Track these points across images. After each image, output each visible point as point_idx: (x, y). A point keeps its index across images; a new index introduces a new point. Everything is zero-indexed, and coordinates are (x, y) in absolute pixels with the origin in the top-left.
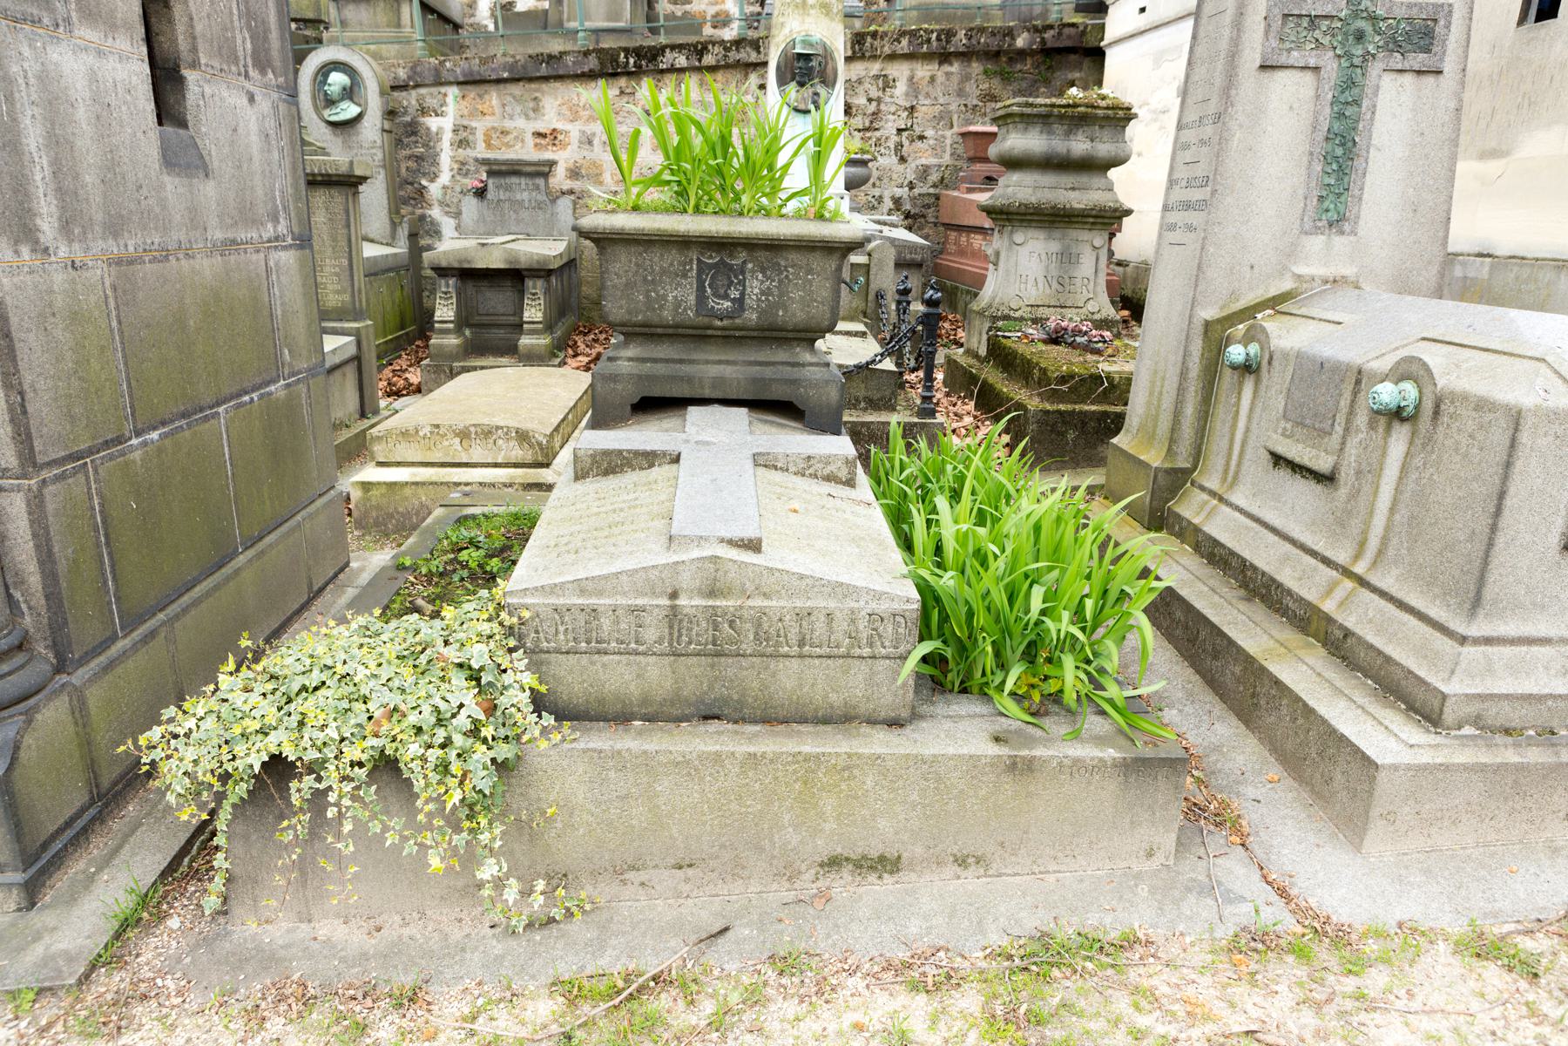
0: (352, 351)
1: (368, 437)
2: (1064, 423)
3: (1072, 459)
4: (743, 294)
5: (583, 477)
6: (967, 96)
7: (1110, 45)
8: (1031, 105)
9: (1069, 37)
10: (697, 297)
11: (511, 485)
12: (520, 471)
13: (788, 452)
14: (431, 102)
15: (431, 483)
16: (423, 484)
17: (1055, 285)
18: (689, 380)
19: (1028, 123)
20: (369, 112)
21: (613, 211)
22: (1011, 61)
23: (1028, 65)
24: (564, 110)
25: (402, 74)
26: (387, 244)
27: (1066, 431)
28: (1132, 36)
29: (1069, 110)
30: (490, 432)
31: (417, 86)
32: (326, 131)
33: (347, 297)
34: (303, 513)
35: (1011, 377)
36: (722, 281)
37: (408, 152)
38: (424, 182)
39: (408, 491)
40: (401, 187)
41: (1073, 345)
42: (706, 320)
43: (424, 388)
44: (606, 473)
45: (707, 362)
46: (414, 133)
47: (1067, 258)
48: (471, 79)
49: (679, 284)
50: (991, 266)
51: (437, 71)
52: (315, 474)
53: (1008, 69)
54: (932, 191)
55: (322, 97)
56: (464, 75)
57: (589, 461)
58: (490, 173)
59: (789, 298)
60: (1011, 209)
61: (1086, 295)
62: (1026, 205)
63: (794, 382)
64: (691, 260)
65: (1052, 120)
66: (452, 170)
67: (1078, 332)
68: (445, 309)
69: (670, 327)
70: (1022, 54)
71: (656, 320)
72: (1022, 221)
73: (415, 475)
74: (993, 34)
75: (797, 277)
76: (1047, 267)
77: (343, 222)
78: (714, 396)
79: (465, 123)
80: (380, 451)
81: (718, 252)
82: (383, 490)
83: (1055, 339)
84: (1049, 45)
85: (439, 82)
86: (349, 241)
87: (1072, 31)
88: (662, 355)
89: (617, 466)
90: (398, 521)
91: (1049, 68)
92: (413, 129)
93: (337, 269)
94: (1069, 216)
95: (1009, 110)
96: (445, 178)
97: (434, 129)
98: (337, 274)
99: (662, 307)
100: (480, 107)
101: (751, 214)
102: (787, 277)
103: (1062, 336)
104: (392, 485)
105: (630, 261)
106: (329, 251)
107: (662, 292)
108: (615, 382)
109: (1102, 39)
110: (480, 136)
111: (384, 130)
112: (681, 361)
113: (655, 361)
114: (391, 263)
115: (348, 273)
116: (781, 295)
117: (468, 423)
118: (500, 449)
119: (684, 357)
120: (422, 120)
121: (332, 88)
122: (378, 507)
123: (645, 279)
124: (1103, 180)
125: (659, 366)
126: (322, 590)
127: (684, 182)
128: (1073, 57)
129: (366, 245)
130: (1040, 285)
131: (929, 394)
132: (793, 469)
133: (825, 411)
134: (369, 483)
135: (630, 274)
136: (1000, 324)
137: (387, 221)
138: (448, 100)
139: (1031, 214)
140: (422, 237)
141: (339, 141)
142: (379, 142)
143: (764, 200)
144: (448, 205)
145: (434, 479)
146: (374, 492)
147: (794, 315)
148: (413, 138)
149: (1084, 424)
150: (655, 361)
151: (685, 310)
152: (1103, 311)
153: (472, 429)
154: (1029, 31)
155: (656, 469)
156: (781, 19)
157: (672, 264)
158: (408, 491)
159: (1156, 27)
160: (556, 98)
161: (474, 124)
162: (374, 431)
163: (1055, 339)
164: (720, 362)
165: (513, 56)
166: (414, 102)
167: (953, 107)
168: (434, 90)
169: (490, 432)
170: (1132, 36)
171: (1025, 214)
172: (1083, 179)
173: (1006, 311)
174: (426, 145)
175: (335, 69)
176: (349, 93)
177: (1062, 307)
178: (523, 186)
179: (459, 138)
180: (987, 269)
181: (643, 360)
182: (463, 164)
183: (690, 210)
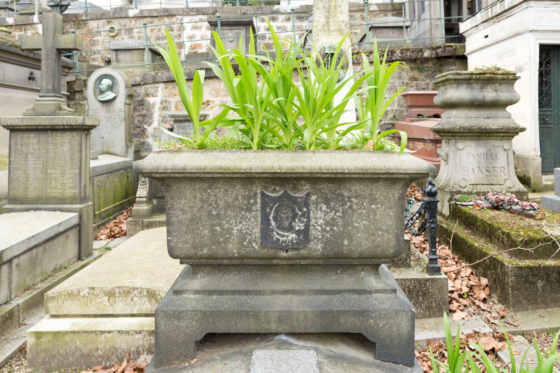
0: (76, 221)
1: (45, 297)
2: (534, 275)
3: (543, 301)
4: (307, 226)
6: (403, 79)
7: (470, 53)
8: (459, 74)
9: (449, 51)
10: (262, 230)
11: (140, 332)
14: (151, 91)
15: (84, 332)
16: (79, 332)
17: (485, 172)
18: (255, 315)
19: (458, 84)
20: (119, 96)
21: (179, 151)
22: (422, 63)
23: (430, 64)
24: (213, 92)
25: (138, 79)
26: (123, 156)
27: (536, 281)
28: (482, 48)
29: (481, 76)
30: (129, 292)
31: (145, 84)
32: (99, 105)
33: (76, 191)
35: (474, 233)
36: (286, 214)
37: (139, 113)
38: (145, 127)
40: (134, 129)
41: (510, 211)
42: (271, 252)
43: (128, 233)
45: (273, 292)
46: (142, 105)
47: (490, 156)
48: (170, 80)
49: (244, 218)
50: (442, 162)
51: (154, 78)
53: (421, 66)
54: (390, 122)
55: (98, 90)
56: (167, 79)
58: (175, 121)
59: (354, 227)
60: (455, 130)
61: (504, 177)
62: (463, 128)
63: (363, 313)
64: (256, 194)
65: (472, 81)
66: (159, 120)
67: (511, 203)
68: (142, 190)
69: (236, 258)
70: (427, 60)
71: (221, 253)
72: (461, 136)
73: (74, 325)
74: (413, 51)
75: (361, 206)
76: (479, 162)
77: (78, 150)
79: (166, 99)
80: (51, 305)
81: (282, 185)
82: (50, 337)
83: (497, 206)
84: (440, 55)
85: (155, 82)
86: (81, 160)
87: (450, 48)
88: (228, 286)
91: (440, 65)
92: (142, 103)
93: (72, 175)
94: (488, 133)
95: (448, 77)
96: (155, 124)
97: (151, 102)
98: (72, 178)
99: (226, 241)
100: (173, 92)
101: (312, 148)
102: (351, 207)
103: (502, 205)
104: (57, 334)
105: (195, 197)
106: (69, 165)
107: (226, 226)
108: (179, 319)
109: (465, 51)
110: (173, 105)
111: (126, 104)
112: (247, 293)
113: (221, 293)
114: (122, 166)
115: (78, 177)
116: (345, 225)
117: (114, 286)
118: (136, 304)
119: (251, 288)
120: (146, 99)
121: (103, 86)
122: (46, 351)
123: (210, 214)
124: (505, 113)
125: (226, 297)
127: (247, 121)
128: (451, 60)
129: (91, 162)
130: (476, 172)
131: (434, 257)
133: (396, 342)
134: (41, 333)
135: (195, 210)
136: (457, 197)
137: (124, 145)
138: (159, 89)
139: (467, 133)
140: (143, 152)
141: (104, 109)
142: (123, 109)
143: (324, 135)
144: (156, 137)
145: (87, 328)
146: (44, 339)
147: (359, 244)
148: (142, 107)
149: (548, 276)
150: (221, 293)
151: (250, 242)
152: (516, 186)
153: (117, 290)
154: (429, 49)
156: (317, 38)
157: (236, 199)
158: (67, 338)
159: (497, 43)
160: (209, 87)
161: (170, 100)
162: (50, 293)
163: (497, 206)
164: (286, 292)
165: (190, 70)
166: (143, 91)
167: (397, 84)
168: (153, 86)
169: (129, 292)
170: (482, 48)
171: (463, 133)
172: (493, 112)
173: (458, 189)
174: (147, 110)
175: (105, 78)
176: (111, 88)
177: (491, 185)
178: (191, 127)
179: (163, 106)
180: (440, 161)
181: (210, 292)
182: (164, 118)
183: (255, 147)
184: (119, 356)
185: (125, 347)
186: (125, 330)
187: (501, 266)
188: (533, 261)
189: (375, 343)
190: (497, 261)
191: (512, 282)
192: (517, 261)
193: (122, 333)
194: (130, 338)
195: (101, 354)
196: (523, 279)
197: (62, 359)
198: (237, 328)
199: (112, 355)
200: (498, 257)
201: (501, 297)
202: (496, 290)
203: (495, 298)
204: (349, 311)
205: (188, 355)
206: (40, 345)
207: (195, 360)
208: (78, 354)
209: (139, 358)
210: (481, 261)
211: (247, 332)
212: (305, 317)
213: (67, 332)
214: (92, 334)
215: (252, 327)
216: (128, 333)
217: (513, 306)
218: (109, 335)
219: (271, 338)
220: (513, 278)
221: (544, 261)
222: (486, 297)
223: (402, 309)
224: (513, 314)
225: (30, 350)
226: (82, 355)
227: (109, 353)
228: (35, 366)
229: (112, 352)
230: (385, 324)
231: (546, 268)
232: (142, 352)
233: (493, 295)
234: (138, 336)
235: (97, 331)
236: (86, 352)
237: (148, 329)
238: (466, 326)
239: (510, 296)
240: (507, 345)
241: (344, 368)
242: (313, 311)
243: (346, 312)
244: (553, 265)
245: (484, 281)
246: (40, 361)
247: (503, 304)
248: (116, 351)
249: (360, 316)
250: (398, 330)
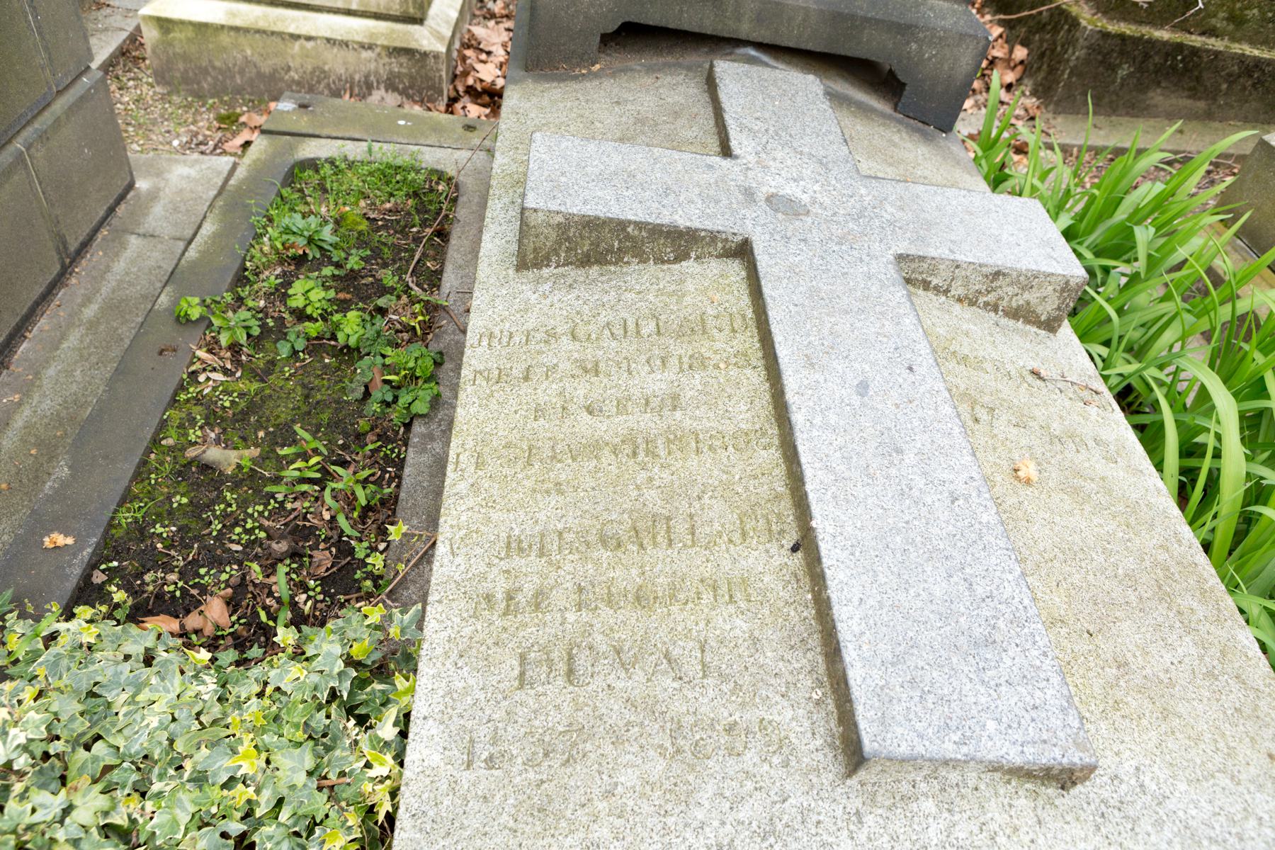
3: (1111, 102)
5: (537, 265)
11: (370, 47)
12: (383, 26)
13: (960, 257)
15: (258, 31)
16: (246, 30)
27: (1119, 66)
34: (28, 133)
39: (225, 39)
44: (586, 262)
52: (41, 58)
57: (553, 236)
73: (233, 15)
78: (755, 36)
82: (190, 33)
89: (610, 251)
90: (215, 79)
122: (185, 57)
126: (85, 245)
132: (958, 290)
145: (262, 25)
146: (176, 35)
149: (1147, 56)
155: (689, 266)
158: (225, 39)
184: (332, 86)
185: (342, 71)
186: (339, 38)
187: (1070, 26)
188: (1133, 27)
189: (904, 85)
190: (1067, 16)
191: (1077, 58)
192: (1105, 21)
193: (334, 44)
194: (350, 56)
195: (296, 77)
196: (1100, 58)
197: (220, 77)
198: (680, 20)
199: (319, 82)
200: (1071, 9)
201: (1041, 84)
202: (1036, 72)
203: (1027, 87)
204: (883, 21)
205: (586, 57)
206: (170, 44)
207: (598, 66)
208: (250, 72)
209: (370, 94)
210: (1034, 12)
211: (697, 30)
212: (804, 20)
213: (223, 27)
214: (273, 38)
215: (707, 22)
216: (347, 46)
217: (1057, 104)
218: (310, 45)
219: (728, 51)
220: (1084, 51)
221: (1152, 30)
222: (1014, 83)
223: (972, 32)
224: (1050, 115)
225: (154, 51)
226: (260, 75)
227: (312, 79)
228: (167, 83)
229: (318, 77)
230: (934, 56)
231: (1152, 43)
232: (375, 84)
233: (1026, 81)
234: (366, 54)
235: (284, 33)
236: (267, 71)
237: (386, 43)
238: (966, 122)
239: (1062, 84)
240: (1025, 161)
241: (852, 112)
242: (822, 11)
243: (878, 22)
244: (1165, 39)
245: (1020, 53)
246: (178, 75)
247: (1038, 98)
248: (325, 77)
249: (899, 33)
250: (952, 69)
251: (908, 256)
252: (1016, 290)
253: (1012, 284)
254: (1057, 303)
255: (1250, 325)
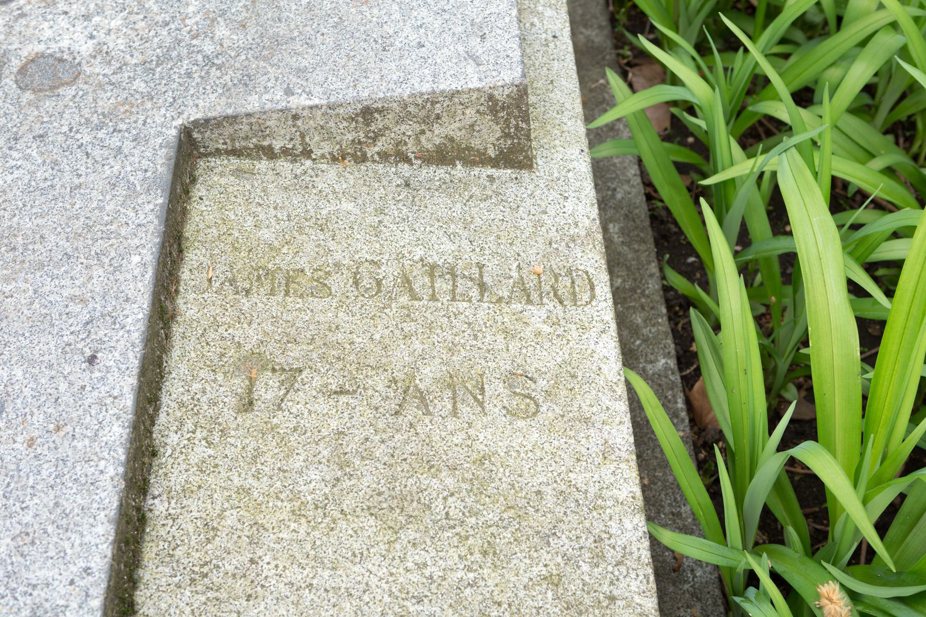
251: (207, 121)
252: (417, 128)
253: (400, 120)
254: (497, 128)
255: (909, 431)
